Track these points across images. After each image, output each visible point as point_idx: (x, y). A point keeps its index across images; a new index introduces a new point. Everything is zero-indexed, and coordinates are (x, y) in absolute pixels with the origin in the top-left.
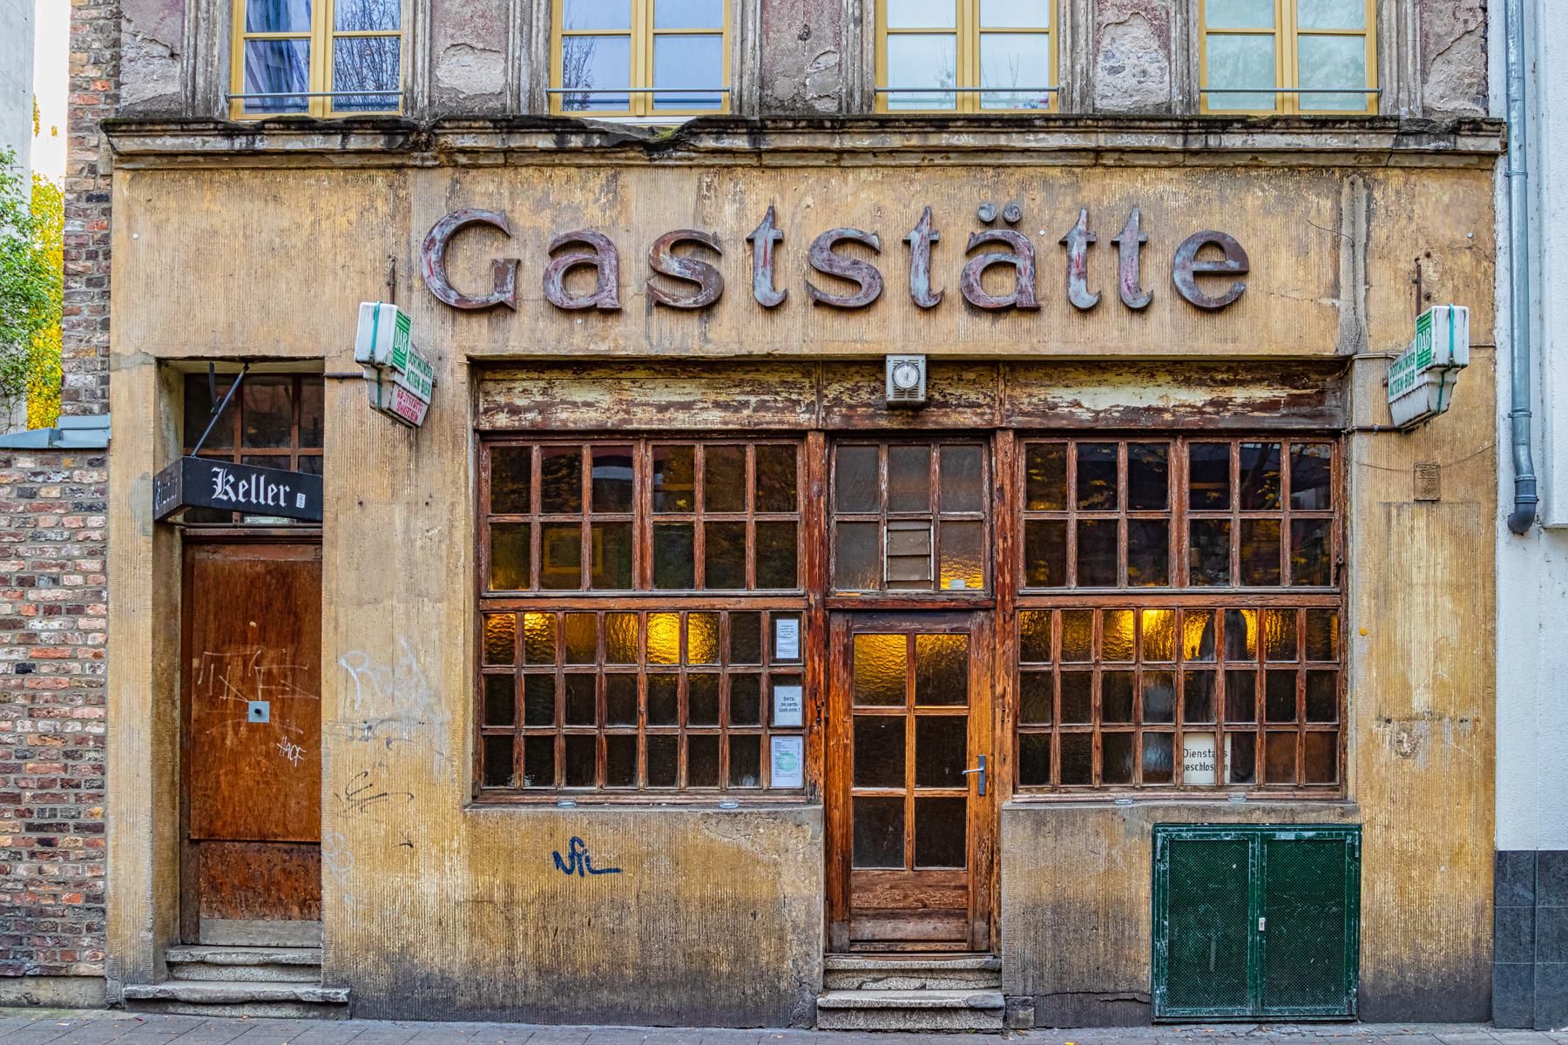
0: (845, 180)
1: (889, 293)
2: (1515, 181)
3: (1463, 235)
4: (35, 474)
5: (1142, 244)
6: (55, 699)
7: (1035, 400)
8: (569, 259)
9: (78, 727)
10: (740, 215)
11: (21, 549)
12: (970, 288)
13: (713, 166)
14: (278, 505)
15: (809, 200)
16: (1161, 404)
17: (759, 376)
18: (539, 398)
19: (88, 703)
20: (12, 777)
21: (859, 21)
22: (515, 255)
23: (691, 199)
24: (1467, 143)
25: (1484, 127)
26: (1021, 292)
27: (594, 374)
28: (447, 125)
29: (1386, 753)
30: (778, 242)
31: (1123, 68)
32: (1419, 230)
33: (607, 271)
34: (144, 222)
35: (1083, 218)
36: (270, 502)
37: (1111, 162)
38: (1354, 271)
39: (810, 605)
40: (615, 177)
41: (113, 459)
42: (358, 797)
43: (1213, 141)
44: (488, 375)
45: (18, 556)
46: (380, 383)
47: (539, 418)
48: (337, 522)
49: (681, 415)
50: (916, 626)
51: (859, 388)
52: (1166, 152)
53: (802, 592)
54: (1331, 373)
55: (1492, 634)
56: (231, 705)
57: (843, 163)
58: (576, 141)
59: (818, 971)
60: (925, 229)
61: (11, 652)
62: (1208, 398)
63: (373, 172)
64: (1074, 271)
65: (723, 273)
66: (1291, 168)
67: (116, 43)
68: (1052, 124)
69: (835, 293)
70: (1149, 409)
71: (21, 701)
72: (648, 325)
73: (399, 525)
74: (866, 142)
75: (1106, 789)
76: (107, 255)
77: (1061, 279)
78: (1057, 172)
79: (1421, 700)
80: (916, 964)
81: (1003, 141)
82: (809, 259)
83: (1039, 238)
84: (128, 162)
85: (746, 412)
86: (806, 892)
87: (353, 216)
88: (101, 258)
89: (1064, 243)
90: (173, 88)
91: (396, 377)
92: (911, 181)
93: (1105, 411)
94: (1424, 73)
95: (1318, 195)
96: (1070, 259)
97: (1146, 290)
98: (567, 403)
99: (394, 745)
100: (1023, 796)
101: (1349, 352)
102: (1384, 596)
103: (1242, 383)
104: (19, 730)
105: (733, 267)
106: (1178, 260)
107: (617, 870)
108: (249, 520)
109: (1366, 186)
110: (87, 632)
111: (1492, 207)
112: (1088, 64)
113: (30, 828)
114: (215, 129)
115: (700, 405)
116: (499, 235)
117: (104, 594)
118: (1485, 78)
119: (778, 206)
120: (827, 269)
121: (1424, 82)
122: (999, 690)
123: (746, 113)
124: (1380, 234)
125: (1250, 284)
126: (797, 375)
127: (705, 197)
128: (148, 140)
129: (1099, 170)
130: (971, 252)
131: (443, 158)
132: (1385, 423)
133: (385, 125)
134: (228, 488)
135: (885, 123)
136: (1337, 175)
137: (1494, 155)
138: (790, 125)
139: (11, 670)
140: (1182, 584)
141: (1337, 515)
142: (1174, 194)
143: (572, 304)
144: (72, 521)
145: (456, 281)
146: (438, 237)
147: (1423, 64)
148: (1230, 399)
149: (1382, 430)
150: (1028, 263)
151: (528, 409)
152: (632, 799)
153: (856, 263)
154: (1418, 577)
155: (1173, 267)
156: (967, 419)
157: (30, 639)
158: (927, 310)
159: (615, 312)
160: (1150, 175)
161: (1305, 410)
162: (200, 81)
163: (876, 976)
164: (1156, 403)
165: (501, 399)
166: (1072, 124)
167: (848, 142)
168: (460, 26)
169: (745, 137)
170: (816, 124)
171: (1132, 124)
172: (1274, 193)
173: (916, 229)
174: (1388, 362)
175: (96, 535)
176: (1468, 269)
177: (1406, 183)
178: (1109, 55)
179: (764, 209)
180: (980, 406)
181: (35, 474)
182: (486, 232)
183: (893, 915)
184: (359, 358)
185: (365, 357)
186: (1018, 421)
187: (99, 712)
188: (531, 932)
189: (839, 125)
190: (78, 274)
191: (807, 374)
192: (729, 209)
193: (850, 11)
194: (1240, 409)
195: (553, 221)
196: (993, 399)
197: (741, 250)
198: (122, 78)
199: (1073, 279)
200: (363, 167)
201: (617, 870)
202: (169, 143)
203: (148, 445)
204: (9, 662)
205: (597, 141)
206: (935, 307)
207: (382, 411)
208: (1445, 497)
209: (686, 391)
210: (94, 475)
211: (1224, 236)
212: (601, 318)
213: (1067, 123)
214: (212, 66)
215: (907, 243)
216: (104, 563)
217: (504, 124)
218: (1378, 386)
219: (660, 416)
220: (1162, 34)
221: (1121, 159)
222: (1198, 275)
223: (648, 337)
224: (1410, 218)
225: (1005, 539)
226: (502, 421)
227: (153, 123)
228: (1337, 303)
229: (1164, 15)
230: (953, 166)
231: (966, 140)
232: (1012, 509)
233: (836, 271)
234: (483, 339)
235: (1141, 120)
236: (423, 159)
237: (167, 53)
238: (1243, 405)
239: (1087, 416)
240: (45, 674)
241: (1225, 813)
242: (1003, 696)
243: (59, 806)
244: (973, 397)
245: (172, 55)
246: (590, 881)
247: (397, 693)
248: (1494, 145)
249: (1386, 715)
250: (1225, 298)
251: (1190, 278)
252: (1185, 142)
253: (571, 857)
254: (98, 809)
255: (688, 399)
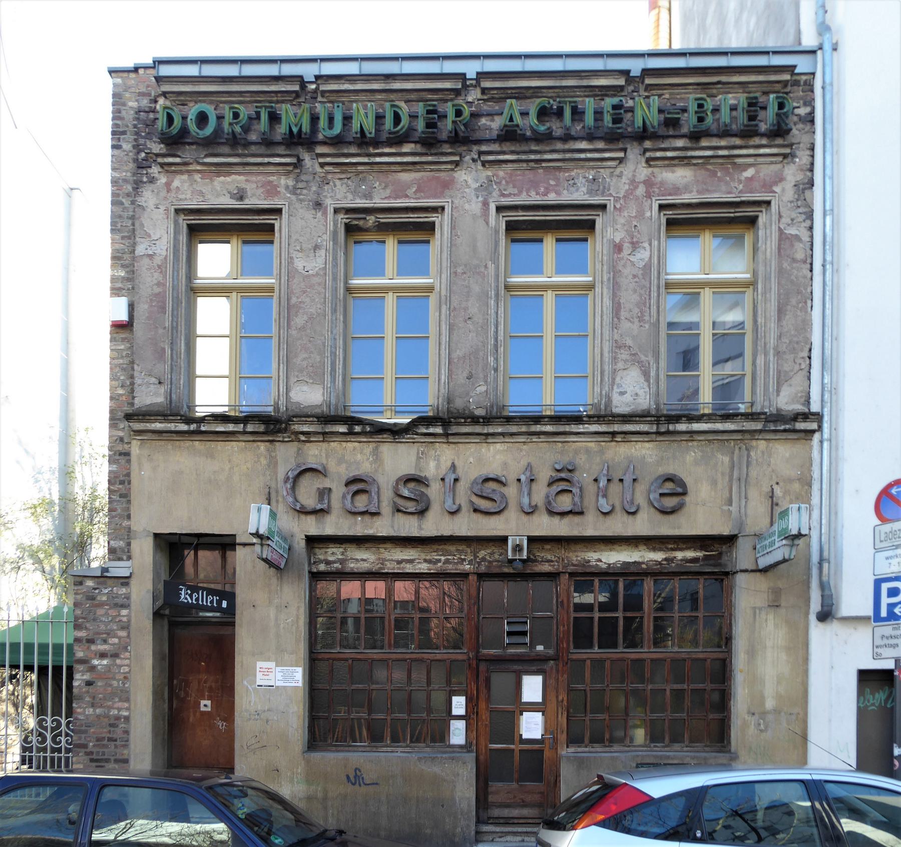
0: (489, 450)
1: (510, 506)
2: (826, 445)
3: (794, 473)
4: (95, 589)
5: (634, 480)
6: (105, 698)
7: (579, 558)
8: (355, 487)
9: (116, 712)
10: (438, 467)
11: (88, 625)
12: (549, 503)
13: (424, 442)
14: (213, 605)
15: (471, 460)
16: (640, 560)
17: (446, 547)
18: (340, 557)
19: (121, 700)
20: (83, 736)
21: (496, 370)
22: (328, 486)
23: (413, 459)
24: (801, 426)
25: (810, 417)
26: (574, 505)
27: (366, 545)
28: (295, 419)
29: (752, 730)
30: (456, 480)
31: (626, 392)
32: (773, 471)
33: (373, 494)
34: (147, 466)
35: (606, 467)
36: (209, 604)
37: (619, 439)
38: (740, 493)
39: (470, 658)
40: (377, 448)
41: (133, 582)
42: (252, 747)
43: (671, 427)
44: (316, 545)
45: (86, 628)
46: (262, 545)
47: (340, 566)
48: (243, 617)
49: (408, 566)
50: (520, 667)
51: (494, 553)
52: (647, 433)
53: (465, 651)
54: (725, 544)
55: (806, 672)
56: (192, 702)
57: (488, 441)
58: (358, 429)
59: (473, 833)
60: (528, 474)
61: (83, 675)
62: (664, 557)
63: (259, 443)
64: (601, 494)
65: (429, 495)
66: (708, 440)
67: (132, 377)
68: (592, 419)
69: (484, 504)
70: (635, 562)
71: (87, 699)
72: (393, 521)
73: (272, 616)
74: (500, 430)
75: (611, 746)
76: (129, 483)
77: (593, 499)
78: (592, 445)
79: (770, 704)
80: (520, 830)
81: (567, 428)
82: (471, 489)
83: (584, 477)
84: (139, 435)
85: (439, 564)
86: (467, 795)
87: (249, 465)
88: (126, 483)
89: (596, 480)
90: (160, 399)
91: (269, 542)
92: (521, 450)
93: (613, 564)
94: (778, 392)
95: (722, 455)
96: (599, 487)
97: (636, 503)
98: (354, 559)
99: (270, 723)
100: (571, 750)
101: (736, 533)
102: (752, 653)
103: (681, 550)
104: (87, 713)
105: (434, 491)
106: (653, 488)
107: (377, 784)
108: (201, 614)
109: (747, 449)
110: (121, 666)
111: (811, 459)
112: (609, 390)
113: (92, 760)
114: (180, 420)
115: (418, 561)
116: (321, 476)
117: (129, 648)
118: (809, 392)
119: (456, 463)
120: (480, 494)
121: (778, 395)
122: (560, 698)
123: (440, 415)
124: (753, 473)
125: (687, 499)
126: (464, 547)
127: (421, 458)
128: (148, 425)
129: (613, 444)
130: (550, 484)
131: (293, 437)
132: (754, 568)
133: (264, 419)
134: (187, 596)
135: (509, 420)
136: (732, 444)
137: (813, 432)
138: (463, 421)
139: (83, 684)
140: (649, 648)
141: (726, 614)
142: (650, 455)
143: (356, 510)
144: (113, 612)
145: (300, 498)
146: (291, 476)
147: (778, 387)
148: (675, 557)
149: (752, 571)
150: (578, 490)
151: (334, 562)
152: (385, 749)
153: (494, 490)
154: (769, 644)
155: (649, 492)
156: (546, 568)
157: (93, 668)
158: (528, 513)
159: (377, 514)
160: (639, 445)
161: (711, 562)
162: (174, 396)
163: (500, 835)
164: (637, 559)
165: (322, 557)
166: (602, 419)
167: (491, 429)
168: (301, 371)
169: (440, 427)
170: (475, 420)
171: (631, 419)
172: (700, 454)
173: (523, 473)
174: (756, 537)
175: (125, 619)
176: (798, 490)
177: (767, 448)
178: (619, 386)
179: (449, 464)
180: (552, 561)
181: (95, 589)
182: (314, 474)
183: (507, 806)
184: (251, 532)
185: (254, 531)
186: (571, 569)
187: (126, 705)
188: (336, 813)
189: (487, 420)
190: (115, 491)
191: (469, 546)
192: (432, 464)
193: (492, 364)
194: (679, 562)
195: (347, 470)
196: (559, 558)
197: (438, 484)
198: (135, 394)
199: (600, 498)
200: (254, 441)
201: (377, 784)
202: (158, 426)
203: (149, 576)
204: (82, 680)
205: (368, 429)
206: (532, 512)
207: (263, 560)
208: (783, 604)
209: (411, 554)
210: (124, 590)
211: (675, 475)
212: (370, 517)
213: (598, 418)
214: (180, 389)
215: (519, 480)
216: (129, 633)
217: (322, 419)
218: (751, 549)
219: (398, 566)
220: (646, 375)
221: (624, 438)
222: (662, 495)
223: (393, 527)
224: (769, 465)
225: (564, 626)
226: (322, 567)
227: (150, 415)
228: (731, 508)
229: (647, 364)
230: (542, 442)
231: (549, 428)
232: (567, 612)
233: (484, 494)
234: (313, 527)
235: (636, 416)
236: (284, 437)
237: (157, 382)
238: (681, 560)
239: (605, 566)
240: (100, 686)
241: (672, 759)
242: (562, 701)
243: (106, 750)
244: (549, 557)
245: (160, 383)
246: (364, 789)
247: (271, 698)
248: (814, 426)
249: (753, 711)
250: (675, 506)
251: (657, 496)
252: (658, 428)
253: (355, 777)
254: (125, 752)
255: (412, 558)
